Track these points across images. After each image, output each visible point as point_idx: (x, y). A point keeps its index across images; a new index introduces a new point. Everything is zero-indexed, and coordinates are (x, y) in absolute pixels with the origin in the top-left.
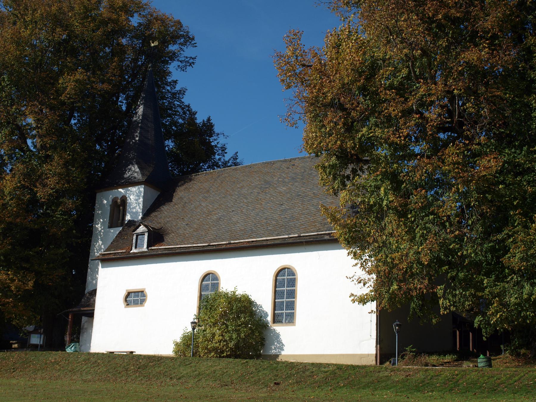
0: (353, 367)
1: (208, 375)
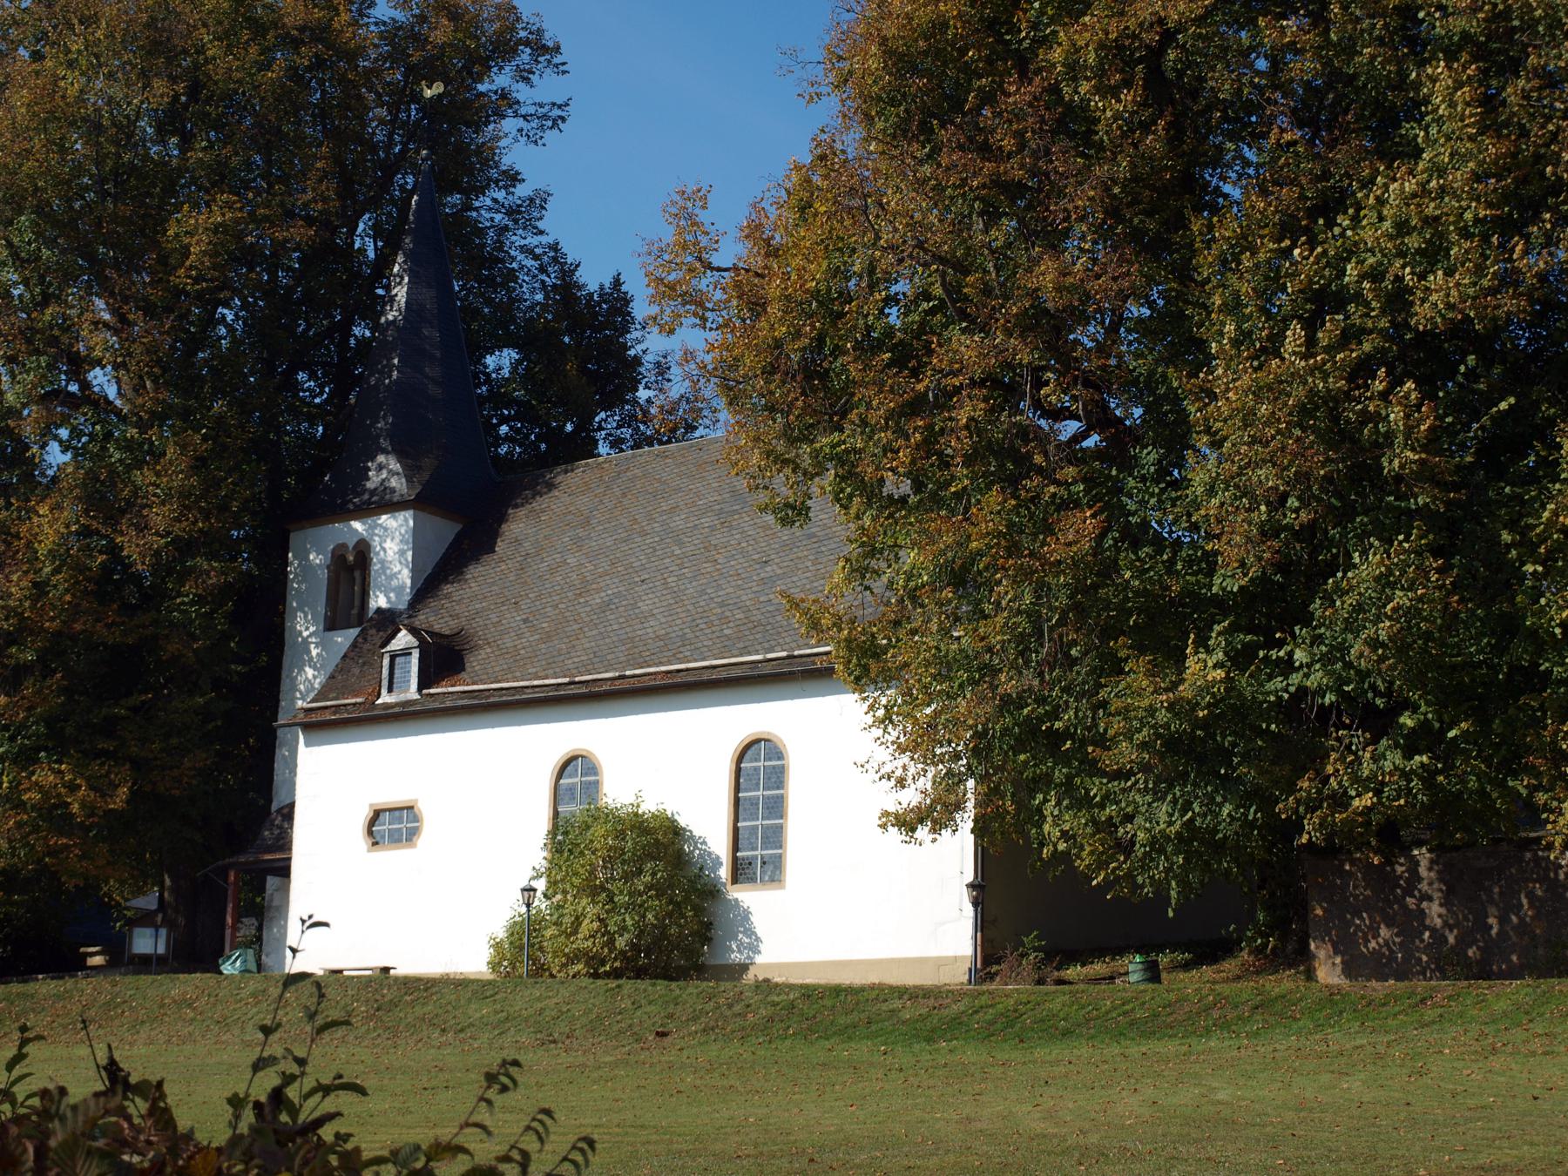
0: (837, 991)
1: (526, 1019)
